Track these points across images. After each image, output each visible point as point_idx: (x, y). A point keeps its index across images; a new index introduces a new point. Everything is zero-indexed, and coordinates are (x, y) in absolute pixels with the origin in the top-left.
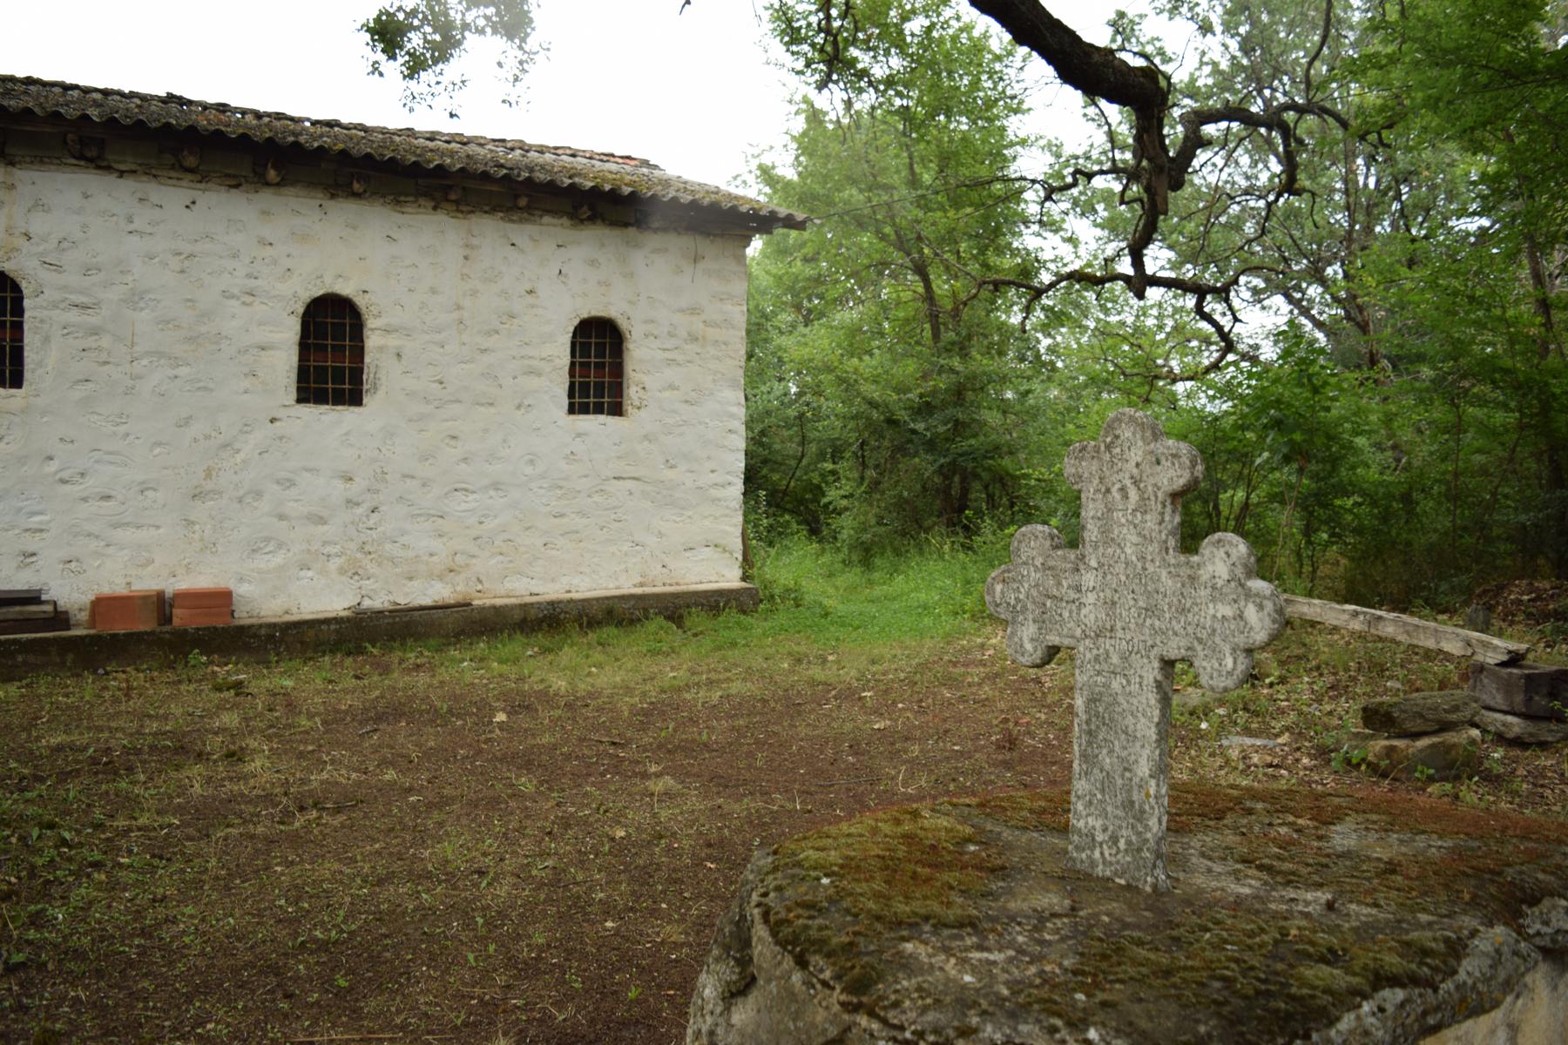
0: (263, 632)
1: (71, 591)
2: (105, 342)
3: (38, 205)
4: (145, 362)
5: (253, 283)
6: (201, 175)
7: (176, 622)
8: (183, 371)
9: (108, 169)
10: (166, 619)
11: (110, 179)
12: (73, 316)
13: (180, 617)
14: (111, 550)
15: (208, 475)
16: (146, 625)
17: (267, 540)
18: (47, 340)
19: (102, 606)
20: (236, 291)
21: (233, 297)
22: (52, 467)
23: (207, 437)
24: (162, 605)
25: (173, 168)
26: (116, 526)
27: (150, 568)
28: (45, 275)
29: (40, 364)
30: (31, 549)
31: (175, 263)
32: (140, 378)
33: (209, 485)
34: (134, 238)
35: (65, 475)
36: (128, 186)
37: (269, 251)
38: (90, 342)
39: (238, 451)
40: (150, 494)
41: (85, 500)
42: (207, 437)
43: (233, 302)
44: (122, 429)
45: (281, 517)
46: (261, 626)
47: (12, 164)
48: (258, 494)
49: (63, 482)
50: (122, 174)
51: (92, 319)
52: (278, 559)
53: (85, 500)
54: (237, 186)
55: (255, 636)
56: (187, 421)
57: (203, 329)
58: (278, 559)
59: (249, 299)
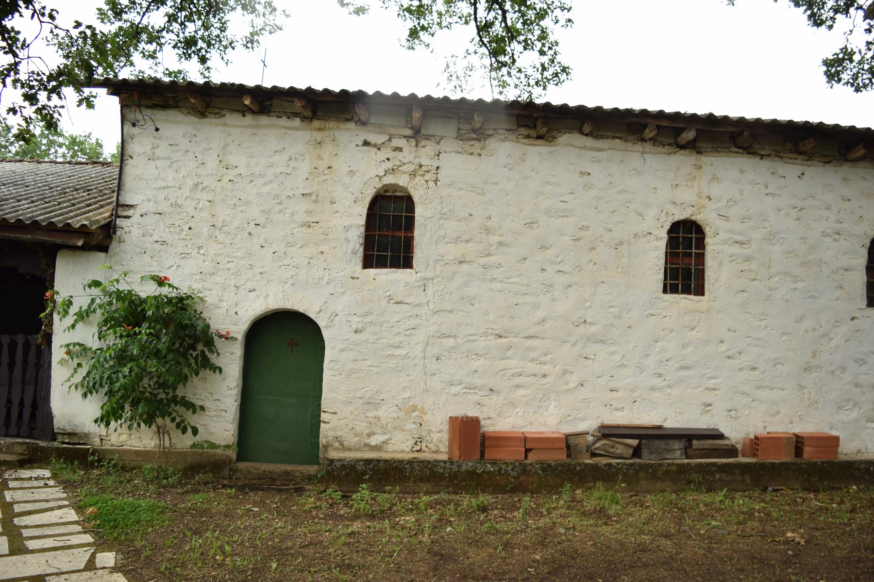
0: (862, 466)
1: (736, 431)
2: (754, 265)
3: (715, 178)
4: (777, 279)
5: (839, 226)
6: (809, 157)
7: (805, 456)
8: (800, 285)
9: (754, 154)
10: (799, 452)
11: (756, 160)
12: (735, 249)
13: (808, 451)
14: (755, 404)
15: (814, 356)
16: (788, 458)
17: (848, 400)
18: (720, 264)
19: (756, 444)
20: (830, 232)
21: (828, 235)
22: (723, 347)
23: (814, 330)
24: (799, 442)
25: (791, 152)
26: (758, 388)
27: (778, 417)
28: (721, 223)
29: (717, 280)
30: (709, 402)
31: (794, 214)
32: (774, 289)
33: (814, 362)
34: (770, 198)
35: (730, 353)
36: (766, 163)
37: (848, 205)
38: (745, 266)
39: (832, 339)
40: (779, 367)
41: (741, 370)
42: (814, 330)
43: (827, 239)
44: (763, 323)
45: (857, 385)
46: (861, 462)
47: (699, 153)
48: (844, 369)
49: (729, 357)
50: (762, 157)
51: (745, 251)
52: (854, 414)
53: (741, 370)
54: (828, 162)
55: (858, 469)
56: (801, 319)
57: (811, 257)
58: (854, 414)
59: (837, 237)
